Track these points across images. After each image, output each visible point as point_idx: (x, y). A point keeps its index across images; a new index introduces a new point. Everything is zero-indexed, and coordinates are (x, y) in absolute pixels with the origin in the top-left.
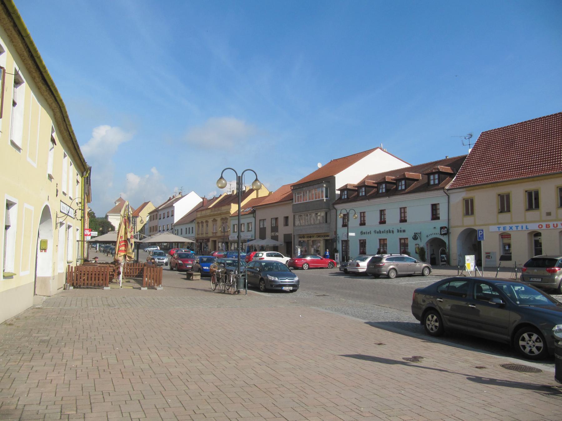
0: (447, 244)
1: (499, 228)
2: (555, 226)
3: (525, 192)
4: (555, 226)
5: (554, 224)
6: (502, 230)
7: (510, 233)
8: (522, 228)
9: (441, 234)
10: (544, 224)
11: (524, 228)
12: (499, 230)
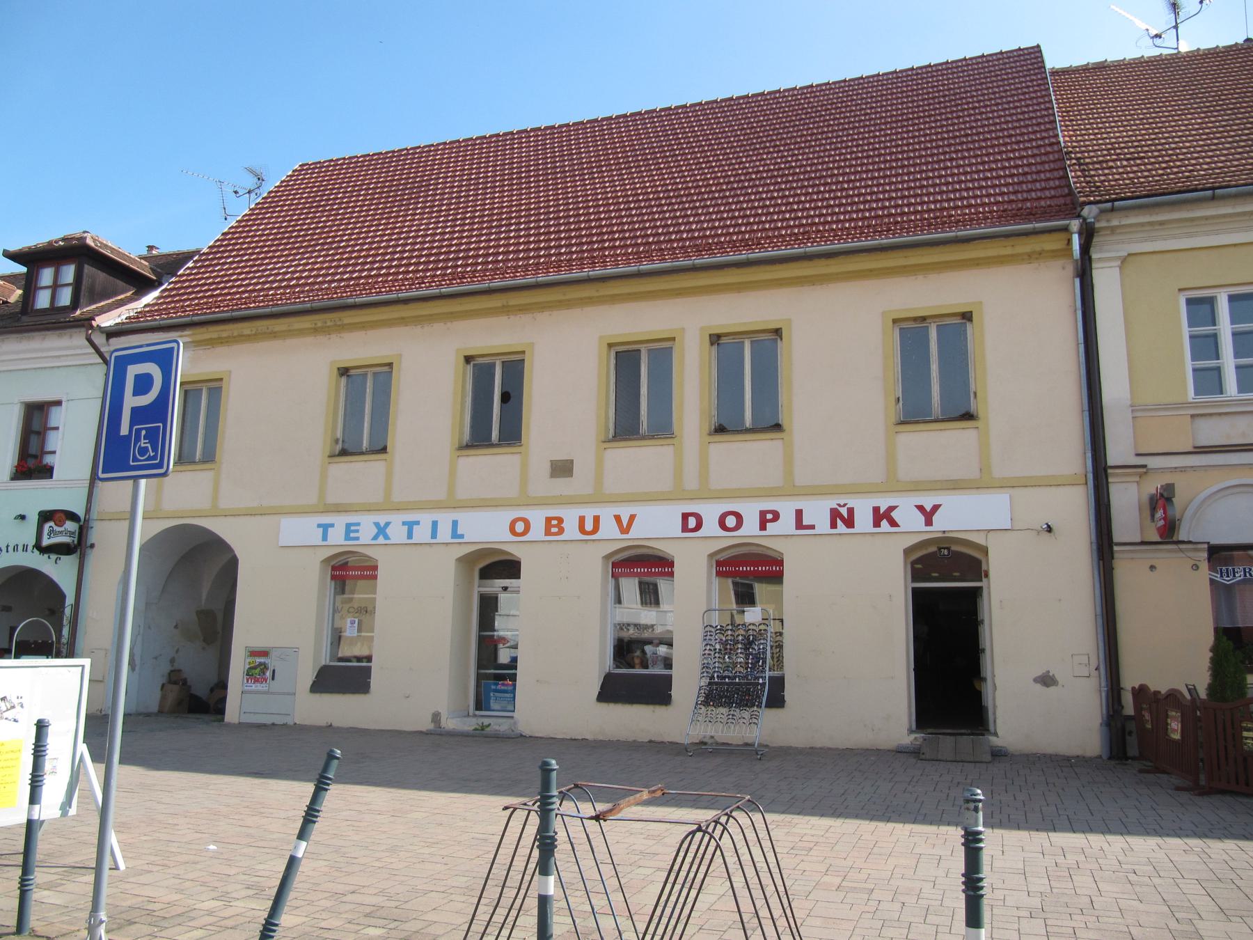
0: (70, 600)
1: (325, 528)
2: (589, 526)
3: (462, 360)
4: (589, 526)
5: (582, 520)
6: (337, 537)
7: (517, 551)
8: (434, 535)
9: (44, 550)
10: (537, 518)
11: (444, 534)
12: (325, 538)
